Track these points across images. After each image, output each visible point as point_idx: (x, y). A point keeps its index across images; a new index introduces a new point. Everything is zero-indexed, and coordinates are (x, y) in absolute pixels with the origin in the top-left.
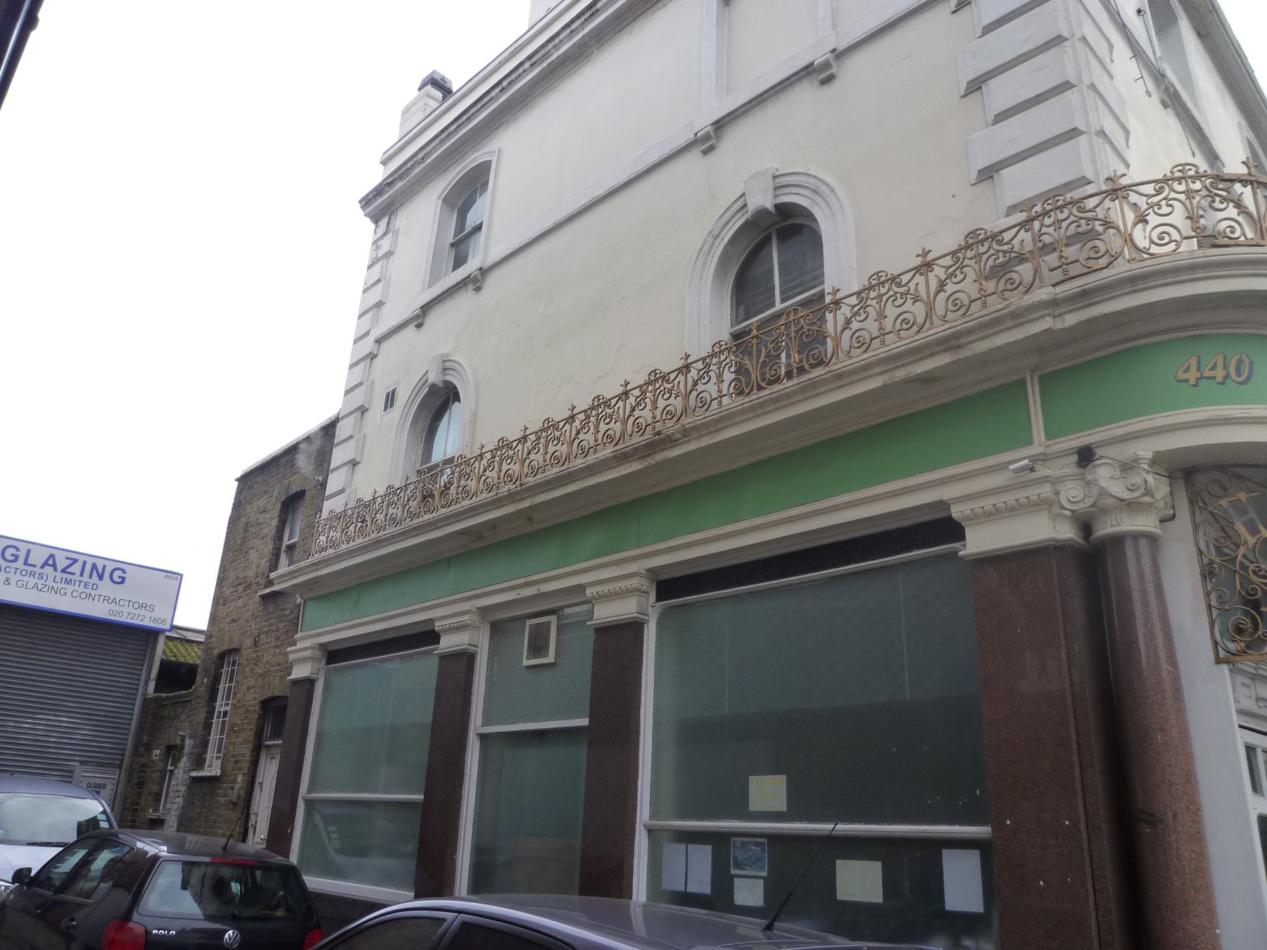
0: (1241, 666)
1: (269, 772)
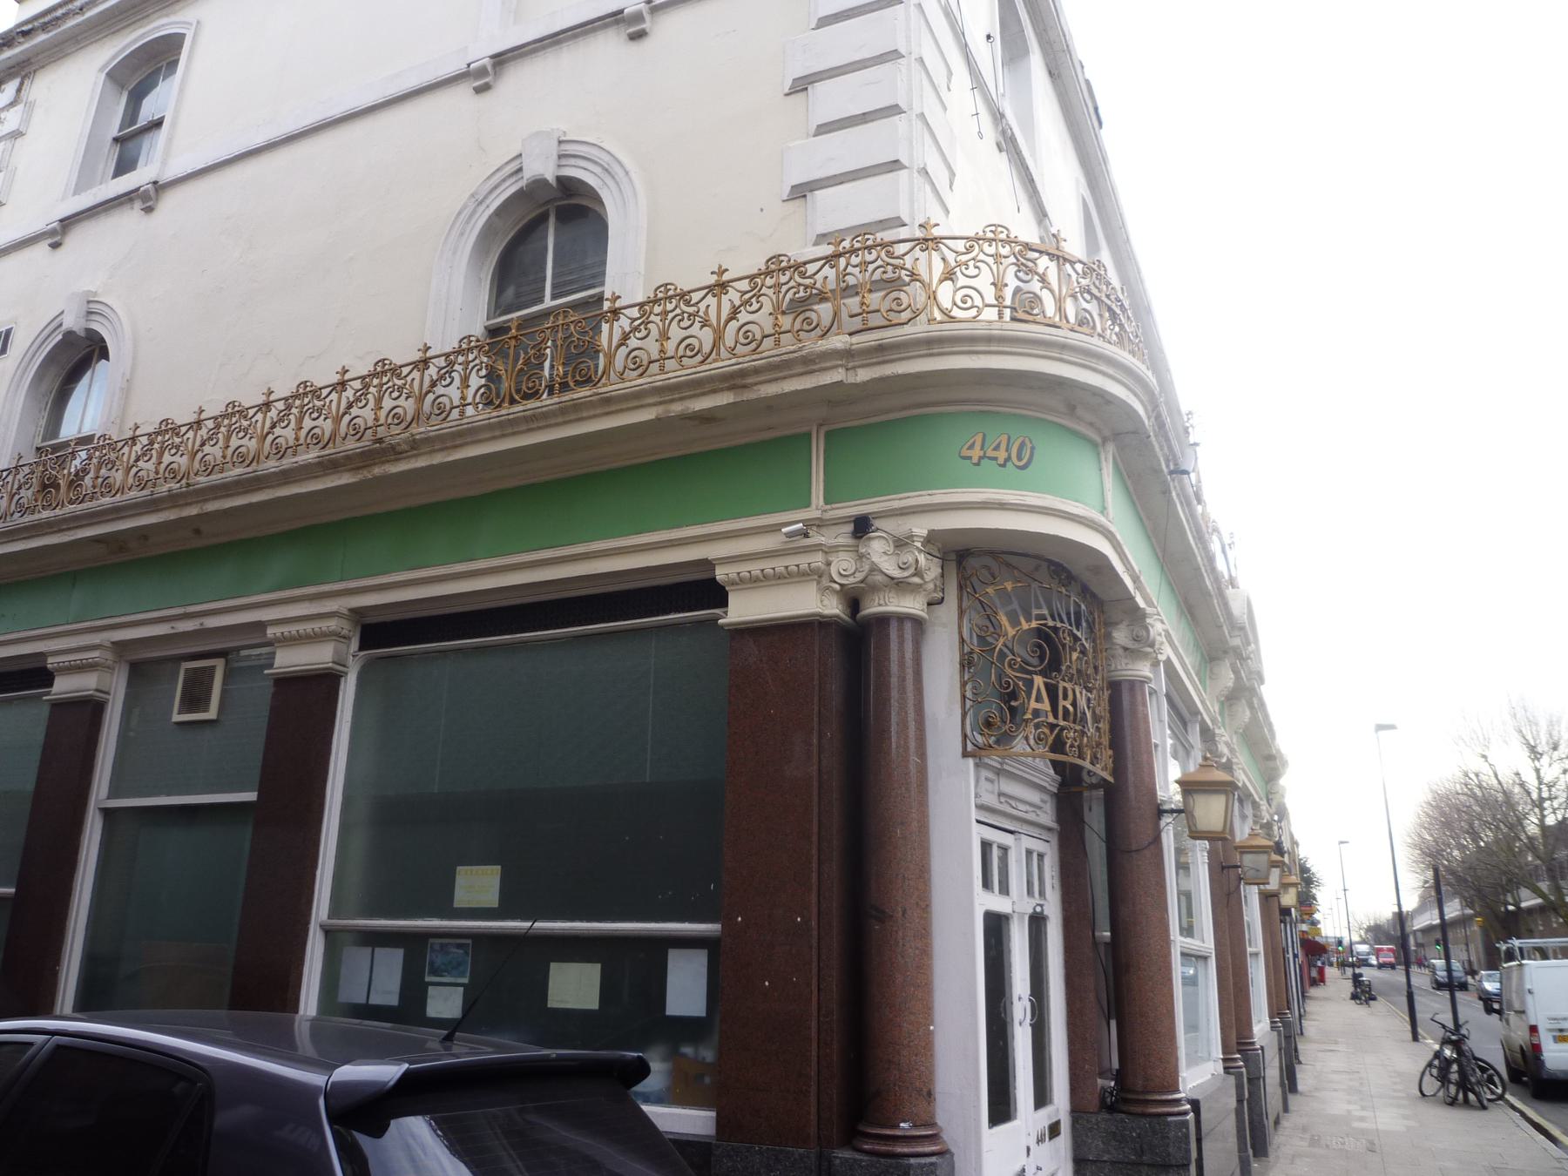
0: (986, 760)
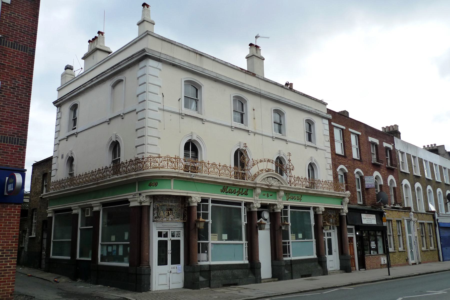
1: (45, 236)
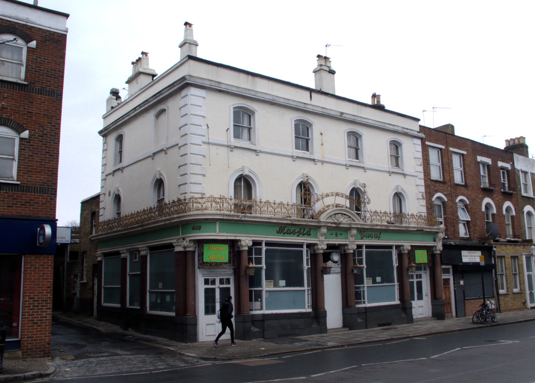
1: (96, 281)
